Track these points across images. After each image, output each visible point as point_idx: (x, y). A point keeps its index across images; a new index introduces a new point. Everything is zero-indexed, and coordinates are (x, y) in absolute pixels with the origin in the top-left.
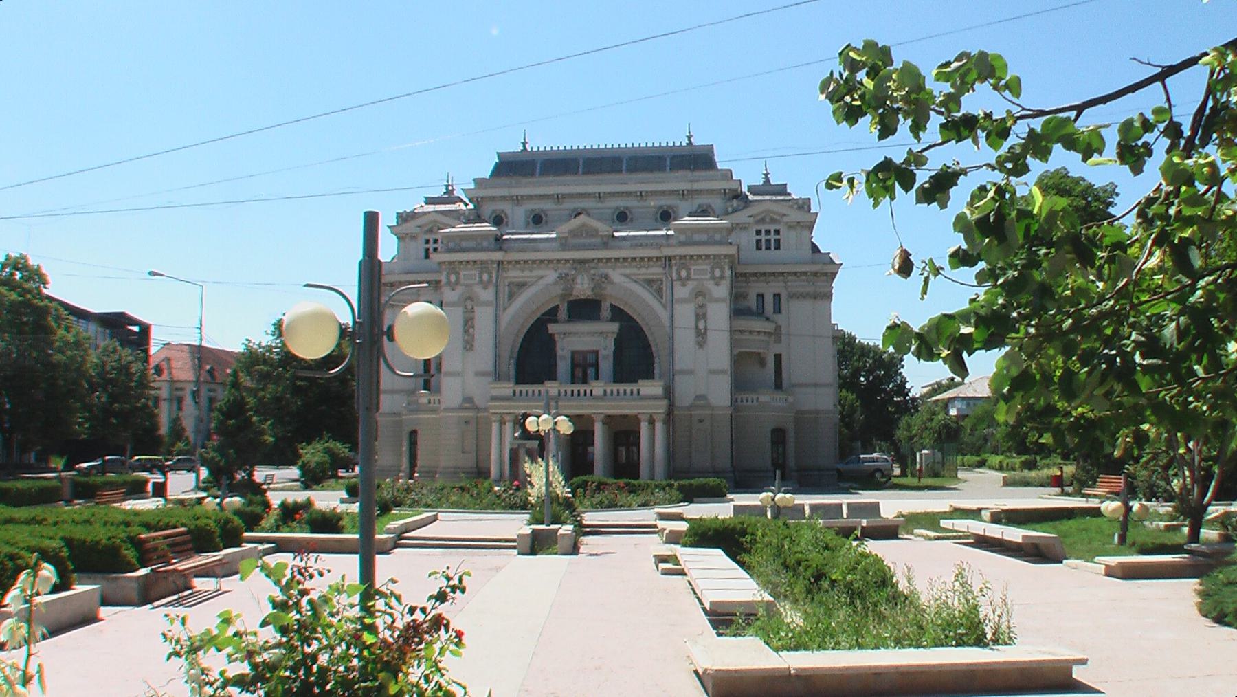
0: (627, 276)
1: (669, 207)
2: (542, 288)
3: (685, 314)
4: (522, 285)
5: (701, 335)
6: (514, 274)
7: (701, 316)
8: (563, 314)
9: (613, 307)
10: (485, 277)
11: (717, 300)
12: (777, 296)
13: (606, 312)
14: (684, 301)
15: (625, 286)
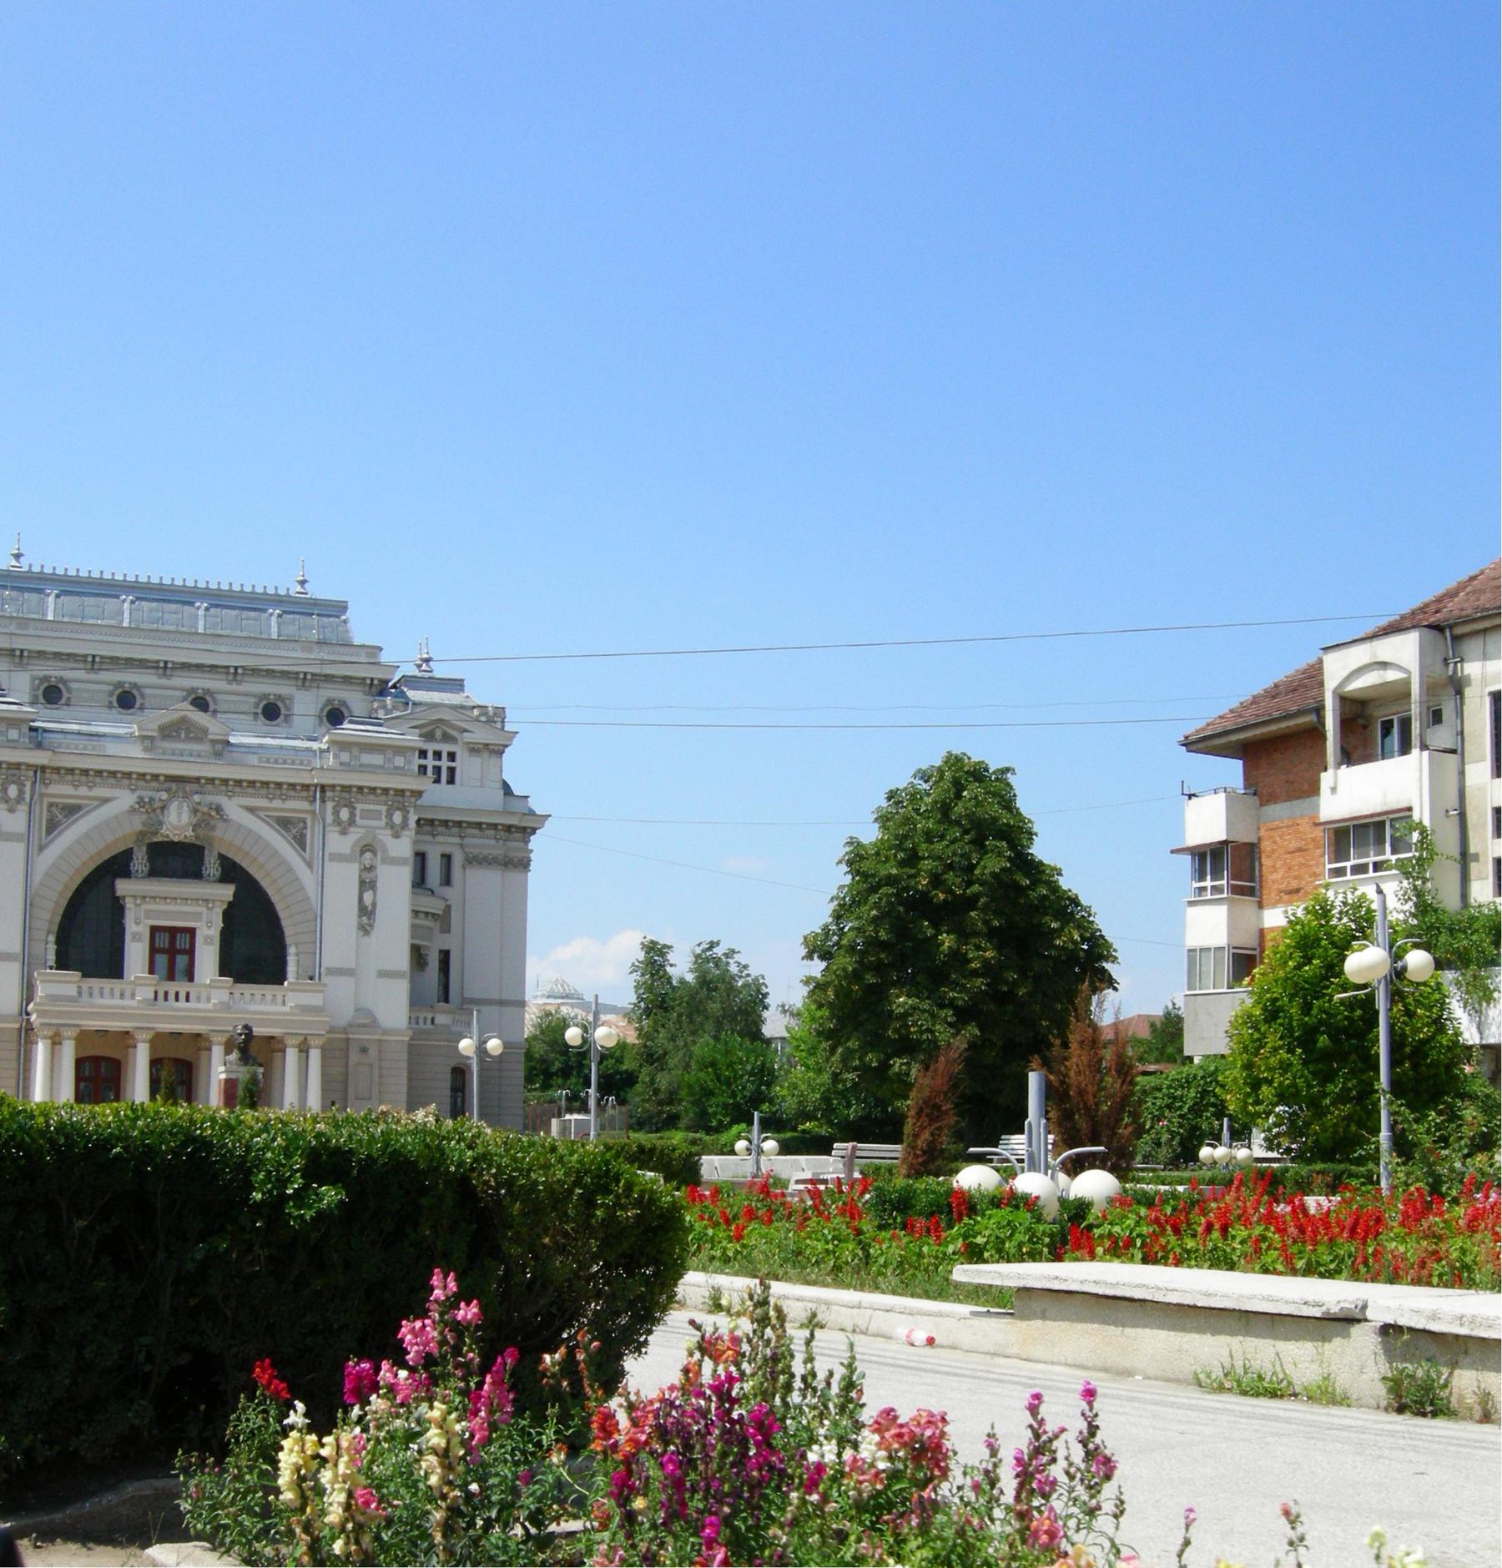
0: (251, 810)
1: (280, 697)
2: (108, 820)
3: (343, 880)
4: (72, 810)
5: (366, 913)
6: (61, 791)
7: (367, 884)
8: (140, 862)
9: (223, 858)
10: (13, 791)
11: (395, 861)
12: (447, 858)
13: (212, 867)
14: (338, 858)
15: (248, 830)
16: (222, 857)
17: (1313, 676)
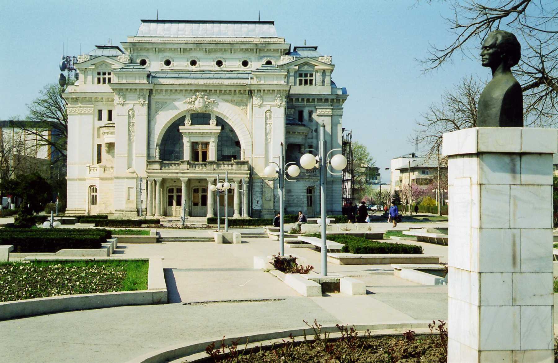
2: (182, 106)
8: (188, 121)
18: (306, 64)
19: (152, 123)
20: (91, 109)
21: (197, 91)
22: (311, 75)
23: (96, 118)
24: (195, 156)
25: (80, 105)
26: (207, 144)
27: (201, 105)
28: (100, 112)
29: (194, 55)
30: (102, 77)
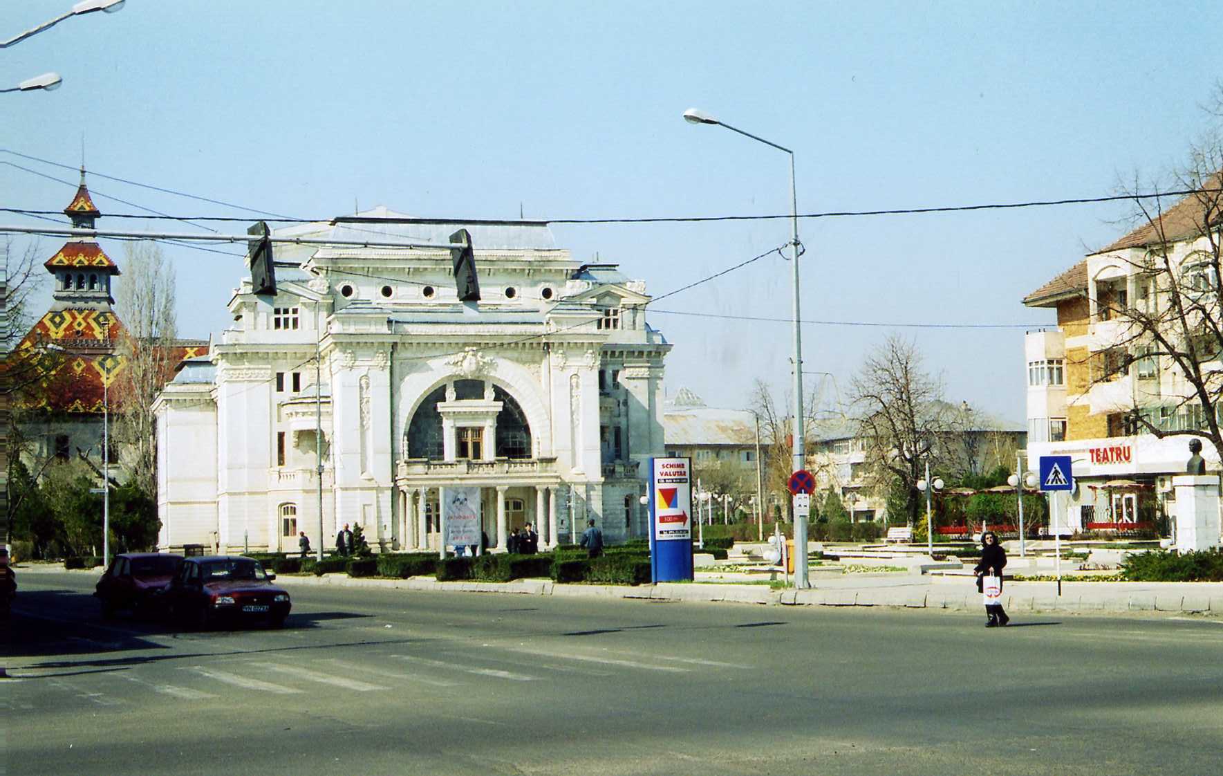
2: (439, 370)
8: (450, 394)
16: (494, 386)
17: (1082, 271)
18: (608, 294)
19: (396, 397)
20: (267, 372)
21: (465, 344)
22: (615, 312)
23: (275, 387)
24: (462, 450)
25: (247, 365)
26: (478, 431)
27: (473, 367)
28: (280, 377)
29: (429, 279)
30: (282, 317)
